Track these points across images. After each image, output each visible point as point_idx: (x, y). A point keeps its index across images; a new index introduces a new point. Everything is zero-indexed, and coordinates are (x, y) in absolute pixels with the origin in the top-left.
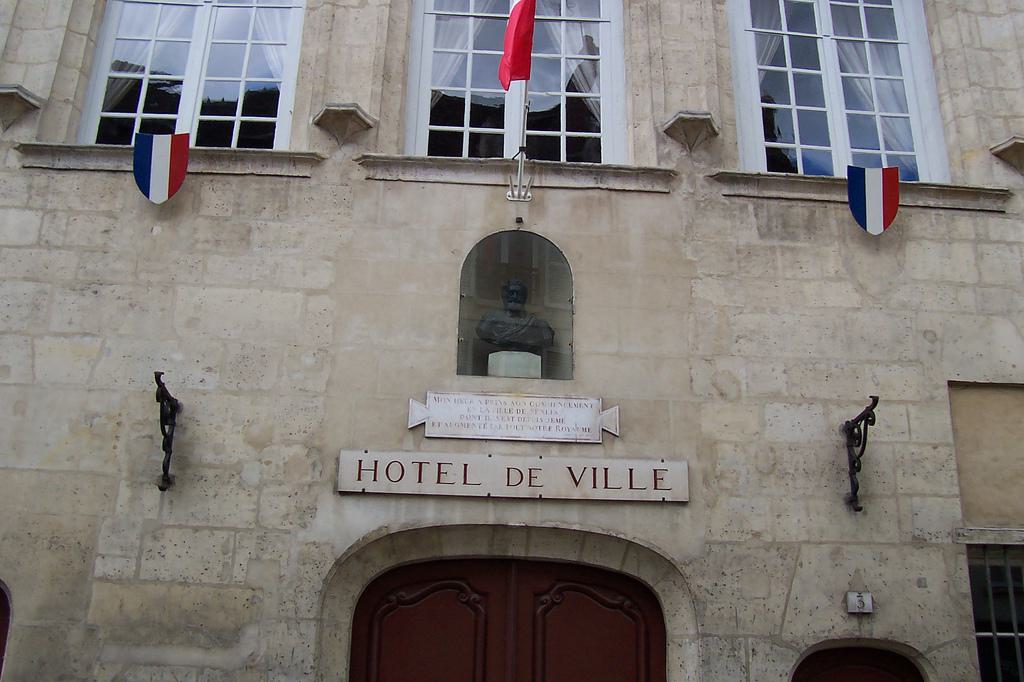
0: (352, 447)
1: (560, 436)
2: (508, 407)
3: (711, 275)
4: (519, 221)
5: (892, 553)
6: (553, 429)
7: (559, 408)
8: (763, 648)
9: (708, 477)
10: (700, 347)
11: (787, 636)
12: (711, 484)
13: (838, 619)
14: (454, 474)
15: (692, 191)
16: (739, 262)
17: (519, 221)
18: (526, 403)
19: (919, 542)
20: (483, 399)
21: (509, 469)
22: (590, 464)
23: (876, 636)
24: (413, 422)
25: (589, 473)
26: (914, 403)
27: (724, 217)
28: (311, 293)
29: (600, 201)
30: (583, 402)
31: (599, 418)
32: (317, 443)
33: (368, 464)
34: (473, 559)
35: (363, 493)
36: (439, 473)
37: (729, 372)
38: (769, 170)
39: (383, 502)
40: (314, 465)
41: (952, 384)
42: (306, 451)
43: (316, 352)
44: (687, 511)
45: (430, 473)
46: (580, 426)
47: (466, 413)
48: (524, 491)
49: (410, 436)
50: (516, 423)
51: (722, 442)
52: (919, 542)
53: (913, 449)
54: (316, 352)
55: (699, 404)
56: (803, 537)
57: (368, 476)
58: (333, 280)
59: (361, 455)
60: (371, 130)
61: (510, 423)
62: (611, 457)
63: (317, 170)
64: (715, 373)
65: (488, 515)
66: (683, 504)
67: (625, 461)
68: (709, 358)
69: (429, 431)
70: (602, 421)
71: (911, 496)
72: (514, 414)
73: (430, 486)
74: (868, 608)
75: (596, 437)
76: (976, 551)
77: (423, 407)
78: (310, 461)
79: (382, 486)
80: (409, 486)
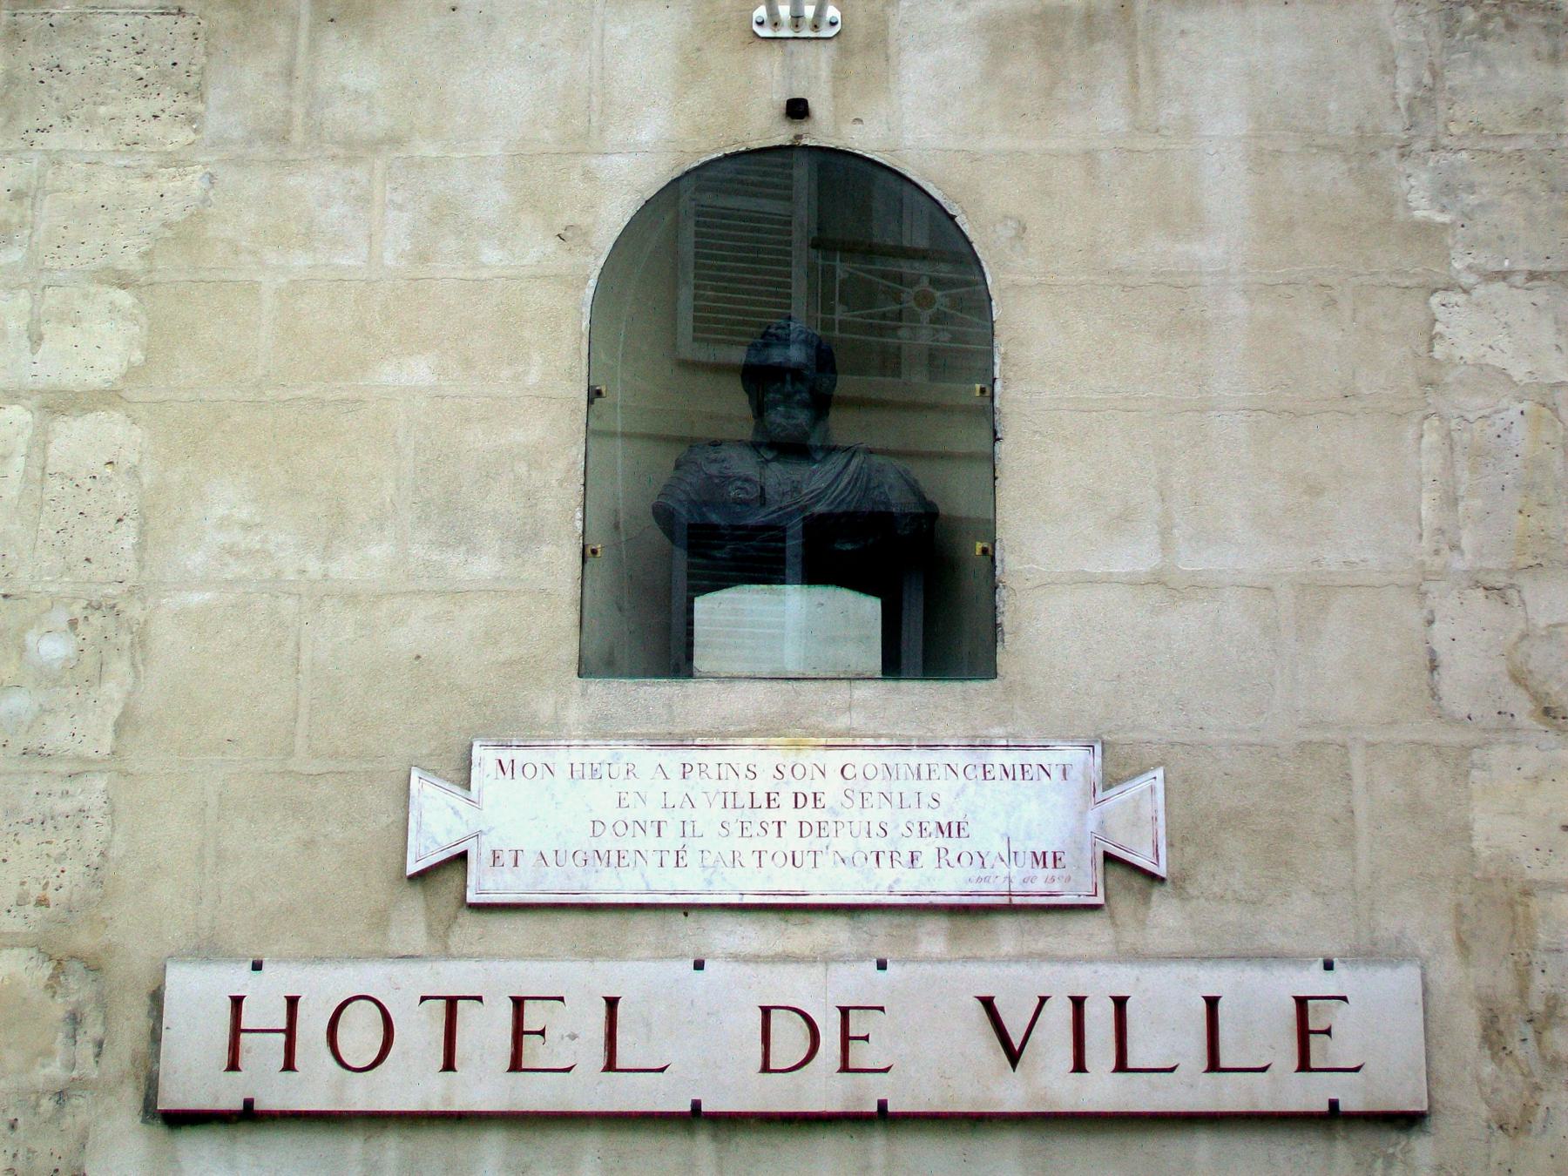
0: (207, 950)
3: (1504, 276)
4: (797, 109)
7: (944, 786)
10: (1466, 541)
12: (1514, 1044)
14: (570, 1034)
17: (797, 109)
18: (823, 769)
20: (673, 759)
21: (766, 1011)
22: (1061, 982)
30: (1034, 757)
31: (1093, 817)
32: (84, 940)
33: (264, 1011)
35: (249, 1116)
36: (518, 1033)
40: (75, 1019)
45: (484, 1032)
47: (610, 814)
48: (822, 1089)
54: (77, 610)
57: (263, 1051)
58: (138, 357)
61: (770, 843)
69: (483, 884)
72: (786, 812)
75: (1081, 884)
77: (456, 798)
78: (58, 1009)
79: (317, 1085)
80: (410, 1083)
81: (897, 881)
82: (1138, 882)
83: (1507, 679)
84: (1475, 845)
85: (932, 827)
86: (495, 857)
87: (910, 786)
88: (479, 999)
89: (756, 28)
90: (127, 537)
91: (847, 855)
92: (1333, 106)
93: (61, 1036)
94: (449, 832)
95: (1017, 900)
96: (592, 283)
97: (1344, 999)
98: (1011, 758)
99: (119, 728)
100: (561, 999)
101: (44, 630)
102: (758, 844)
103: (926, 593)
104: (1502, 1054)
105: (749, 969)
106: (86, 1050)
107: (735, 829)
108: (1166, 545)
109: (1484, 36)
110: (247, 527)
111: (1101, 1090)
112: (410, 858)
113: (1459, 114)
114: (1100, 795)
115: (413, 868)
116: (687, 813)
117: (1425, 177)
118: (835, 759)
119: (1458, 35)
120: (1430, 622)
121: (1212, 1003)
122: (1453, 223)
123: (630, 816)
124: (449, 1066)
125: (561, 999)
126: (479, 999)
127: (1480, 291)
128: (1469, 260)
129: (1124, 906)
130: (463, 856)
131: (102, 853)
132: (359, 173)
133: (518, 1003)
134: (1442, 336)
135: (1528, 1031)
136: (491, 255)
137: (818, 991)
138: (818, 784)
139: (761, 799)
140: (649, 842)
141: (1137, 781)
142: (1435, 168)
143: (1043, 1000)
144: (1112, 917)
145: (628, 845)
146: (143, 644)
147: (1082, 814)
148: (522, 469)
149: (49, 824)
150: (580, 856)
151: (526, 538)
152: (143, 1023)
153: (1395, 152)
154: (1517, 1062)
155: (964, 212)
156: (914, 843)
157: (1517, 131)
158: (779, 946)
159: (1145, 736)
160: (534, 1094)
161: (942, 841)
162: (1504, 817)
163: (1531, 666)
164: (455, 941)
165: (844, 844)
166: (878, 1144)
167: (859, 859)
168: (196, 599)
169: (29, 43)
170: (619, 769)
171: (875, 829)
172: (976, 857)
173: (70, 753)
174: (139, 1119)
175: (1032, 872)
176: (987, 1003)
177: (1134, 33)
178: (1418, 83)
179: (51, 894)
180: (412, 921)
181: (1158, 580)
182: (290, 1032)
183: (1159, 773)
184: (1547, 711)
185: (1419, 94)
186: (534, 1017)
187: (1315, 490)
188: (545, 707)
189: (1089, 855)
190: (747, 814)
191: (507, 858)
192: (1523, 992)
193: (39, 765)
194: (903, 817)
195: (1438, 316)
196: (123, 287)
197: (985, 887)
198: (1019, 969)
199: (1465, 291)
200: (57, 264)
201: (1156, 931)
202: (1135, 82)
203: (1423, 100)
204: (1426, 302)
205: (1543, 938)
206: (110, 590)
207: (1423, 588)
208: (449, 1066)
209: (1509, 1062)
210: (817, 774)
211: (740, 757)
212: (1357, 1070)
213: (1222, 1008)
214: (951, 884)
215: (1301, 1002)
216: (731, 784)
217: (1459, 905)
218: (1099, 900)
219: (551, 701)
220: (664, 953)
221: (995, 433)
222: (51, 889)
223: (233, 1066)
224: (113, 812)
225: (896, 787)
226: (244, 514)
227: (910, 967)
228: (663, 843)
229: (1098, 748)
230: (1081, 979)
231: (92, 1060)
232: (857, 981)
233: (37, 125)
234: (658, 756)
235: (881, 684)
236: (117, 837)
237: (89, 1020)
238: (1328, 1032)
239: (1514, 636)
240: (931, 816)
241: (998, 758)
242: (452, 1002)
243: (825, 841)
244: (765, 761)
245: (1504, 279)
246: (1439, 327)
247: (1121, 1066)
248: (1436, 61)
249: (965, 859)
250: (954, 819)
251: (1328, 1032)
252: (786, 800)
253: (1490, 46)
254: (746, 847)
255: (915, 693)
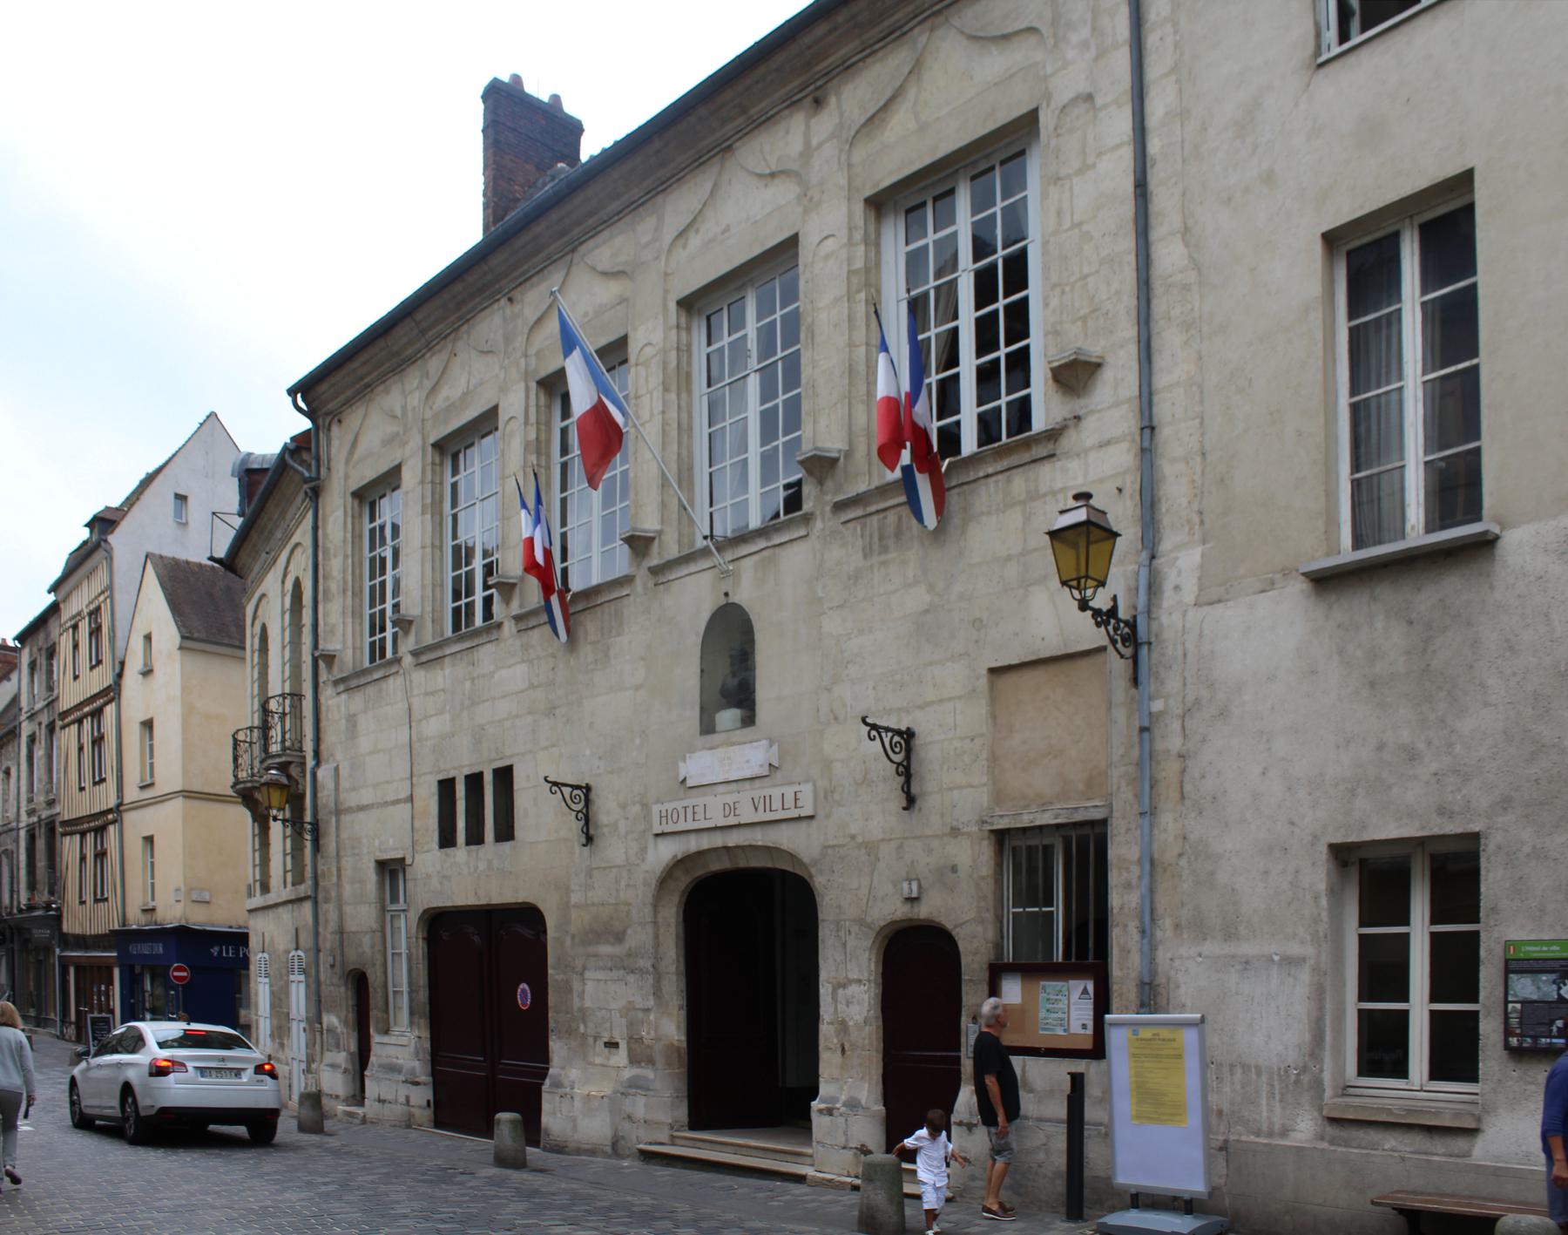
1: (748, 774)
5: (936, 844)
8: (855, 929)
9: (826, 795)
11: (869, 920)
13: (899, 904)
19: (955, 832)
23: (922, 916)
26: (960, 698)
39: (677, 838)
41: (992, 671)
44: (814, 823)
52: (955, 832)
53: (957, 744)
56: (881, 836)
65: (718, 840)
66: (812, 817)
69: (690, 783)
71: (950, 789)
74: (915, 894)
76: (1001, 837)
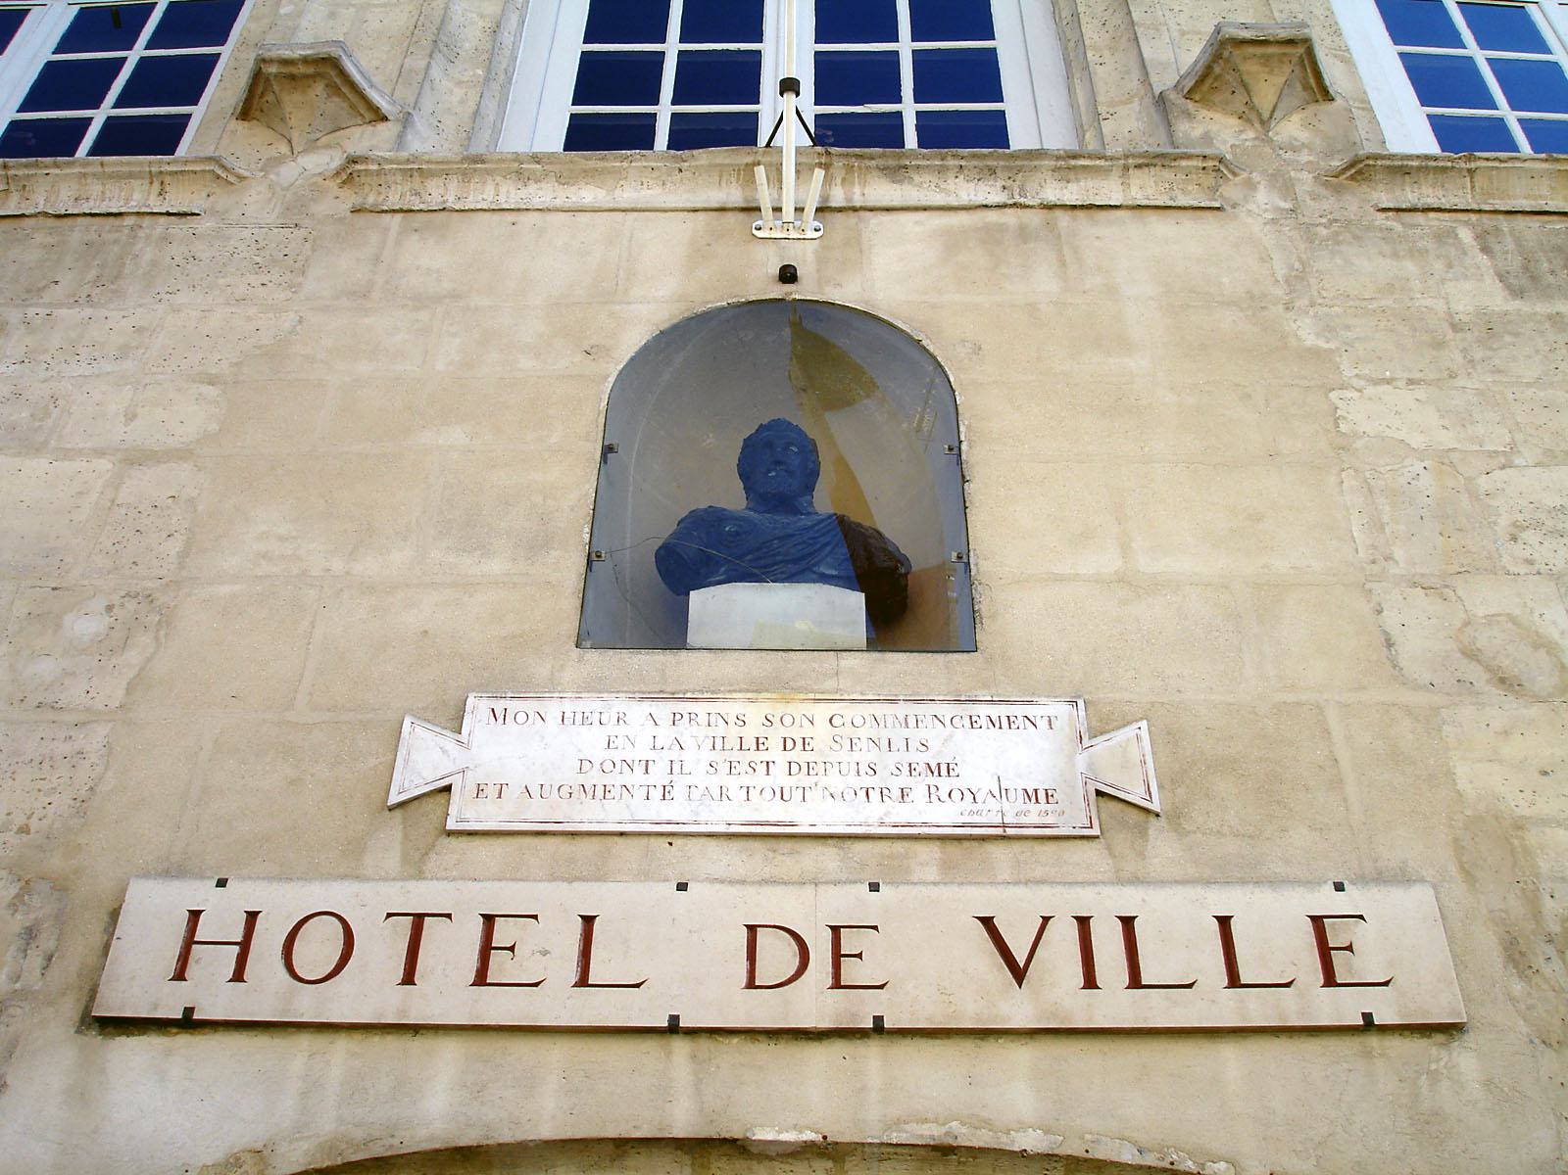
0: (174, 870)
2: (750, 734)
3: (1389, 382)
4: (788, 275)
6: (919, 792)
7: (933, 734)
10: (1399, 553)
12: (1539, 962)
14: (543, 951)
15: (1288, 205)
16: (1464, 350)
17: (788, 275)
18: (814, 719)
20: (663, 710)
21: (752, 929)
22: (1066, 903)
24: (408, 782)
25: (1063, 939)
27: (1395, 255)
28: (137, 458)
29: (1023, 234)
30: (1019, 710)
31: (1081, 761)
32: (56, 863)
33: (222, 921)
34: (581, 1139)
35: (188, 1023)
36: (486, 949)
37: (1512, 619)
38: (1443, 151)
40: (30, 934)
42: (13, 890)
43: (116, 599)
45: (450, 950)
46: (1015, 783)
47: (599, 754)
48: (812, 1002)
49: (393, 832)
50: (780, 777)
51: (1543, 822)
54: (116, 599)
55: (1435, 710)
57: (213, 964)
58: (214, 427)
59: (200, 893)
60: (381, 127)
61: (760, 779)
62: (1136, 880)
63: (222, 200)
64: (1467, 624)
65: (674, 1097)
66: (1450, 1030)
67: (1197, 892)
68: (1438, 582)
69: (463, 812)
70: (1090, 766)
72: (775, 752)
73: (442, 990)
75: (1073, 815)
77: (448, 741)
78: (19, 922)
79: (266, 993)
80: (369, 990)
81: (887, 814)
82: (1134, 816)
83: (1459, 655)
84: (1460, 787)
85: (922, 768)
86: (479, 790)
87: (898, 735)
88: (449, 916)
89: (755, 232)
90: (174, 547)
91: (837, 792)
92: (1225, 280)
93: (13, 948)
94: (435, 768)
95: (1010, 831)
96: (612, 380)
97: (1361, 917)
98: (995, 711)
99: (130, 689)
100: (535, 917)
101: (83, 612)
102: (746, 781)
103: (905, 600)
104: (1529, 972)
105: (733, 891)
106: (36, 960)
107: (724, 768)
108: (1126, 550)
109: (1338, 243)
110: (281, 539)
111: (1115, 1005)
112: (394, 790)
113: (1327, 286)
114: (1086, 742)
115: (394, 798)
116: (675, 754)
117: (1308, 321)
118: (822, 711)
119: (1317, 242)
120: (1380, 612)
121: (1224, 922)
122: (1338, 349)
123: (617, 756)
124: (409, 979)
125: (535, 917)
126: (449, 916)
127: (1371, 390)
128: (1356, 371)
129: (1121, 840)
130: (448, 789)
131: (91, 789)
132: (424, 316)
133: (489, 920)
134: (1344, 418)
135: (1550, 950)
136: (526, 363)
137: (811, 912)
138: (807, 731)
139: (750, 743)
140: (637, 778)
141: (1122, 731)
142: (1315, 316)
143: (1046, 920)
144: (1109, 848)
145: (615, 780)
146: (168, 624)
147: (1071, 758)
148: (538, 499)
149: (46, 766)
150: (565, 791)
151: (538, 544)
152: (97, 939)
153: (1281, 307)
154: (1546, 980)
155: (928, 338)
156: (904, 780)
157: (1377, 296)
158: (767, 872)
159: (1127, 696)
160: (497, 1007)
161: (933, 780)
162: (1497, 759)
163: (1479, 645)
164: (432, 864)
165: (834, 782)
166: (872, 1052)
167: (850, 795)
168: (225, 590)
169: (175, 244)
170: (610, 717)
171: (864, 768)
172: (966, 792)
173: (81, 707)
174: (72, 1031)
175: (1024, 807)
176: (987, 922)
177: (1059, 236)
178: (1291, 268)
179: (34, 824)
180: (389, 844)
181: (1121, 579)
182: (245, 945)
183: (1144, 724)
184: (1502, 681)
185: (1293, 274)
186: (502, 935)
187: (1257, 518)
188: (542, 670)
189: (1081, 793)
190: (736, 755)
191: (492, 792)
192: (1537, 915)
193: (51, 715)
194: (891, 759)
195: (1339, 406)
196: (211, 383)
197: (976, 819)
198: (1020, 891)
199: (1360, 391)
200: (160, 370)
201: (1156, 860)
202: (1063, 263)
203: (1296, 277)
204: (1327, 397)
205: (1544, 866)
206: (149, 584)
207: (1367, 586)
208: (409, 979)
209: (1536, 979)
210: (806, 722)
211: (731, 709)
212: (1386, 984)
213: (1235, 927)
214: (945, 815)
215: (1317, 921)
216: (721, 730)
217: (1456, 840)
218: (1095, 831)
219: (549, 666)
220: (644, 875)
221: (963, 477)
222: (35, 819)
223: (180, 975)
224: (110, 754)
225: (885, 734)
226: (282, 530)
227: (903, 889)
228: (650, 780)
229: (1081, 703)
230: (1085, 900)
231: (38, 971)
232: (846, 902)
233: (167, 289)
234: (647, 707)
235: (866, 655)
236: (109, 774)
237: (44, 936)
238: (1349, 948)
239: (1458, 624)
240: (920, 759)
241: (983, 710)
242: (419, 920)
243: (814, 779)
244: (755, 713)
245: (1388, 383)
246: (1339, 412)
247: (1135, 982)
248: (1304, 256)
249: (956, 795)
250: (943, 761)
251: (1349, 948)
252: (775, 743)
253: (1343, 248)
254: (733, 784)
255: (898, 663)
